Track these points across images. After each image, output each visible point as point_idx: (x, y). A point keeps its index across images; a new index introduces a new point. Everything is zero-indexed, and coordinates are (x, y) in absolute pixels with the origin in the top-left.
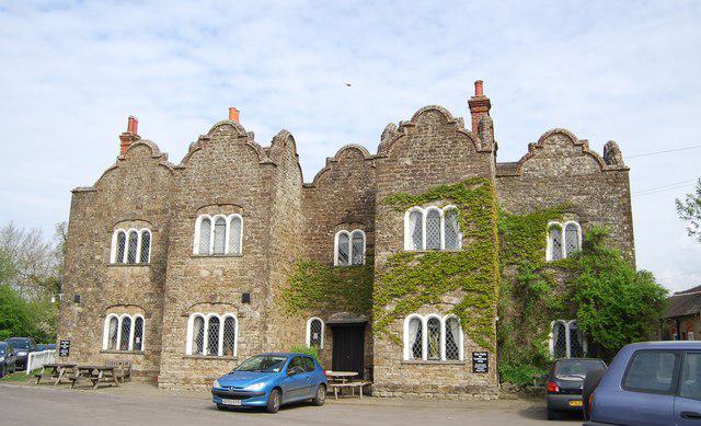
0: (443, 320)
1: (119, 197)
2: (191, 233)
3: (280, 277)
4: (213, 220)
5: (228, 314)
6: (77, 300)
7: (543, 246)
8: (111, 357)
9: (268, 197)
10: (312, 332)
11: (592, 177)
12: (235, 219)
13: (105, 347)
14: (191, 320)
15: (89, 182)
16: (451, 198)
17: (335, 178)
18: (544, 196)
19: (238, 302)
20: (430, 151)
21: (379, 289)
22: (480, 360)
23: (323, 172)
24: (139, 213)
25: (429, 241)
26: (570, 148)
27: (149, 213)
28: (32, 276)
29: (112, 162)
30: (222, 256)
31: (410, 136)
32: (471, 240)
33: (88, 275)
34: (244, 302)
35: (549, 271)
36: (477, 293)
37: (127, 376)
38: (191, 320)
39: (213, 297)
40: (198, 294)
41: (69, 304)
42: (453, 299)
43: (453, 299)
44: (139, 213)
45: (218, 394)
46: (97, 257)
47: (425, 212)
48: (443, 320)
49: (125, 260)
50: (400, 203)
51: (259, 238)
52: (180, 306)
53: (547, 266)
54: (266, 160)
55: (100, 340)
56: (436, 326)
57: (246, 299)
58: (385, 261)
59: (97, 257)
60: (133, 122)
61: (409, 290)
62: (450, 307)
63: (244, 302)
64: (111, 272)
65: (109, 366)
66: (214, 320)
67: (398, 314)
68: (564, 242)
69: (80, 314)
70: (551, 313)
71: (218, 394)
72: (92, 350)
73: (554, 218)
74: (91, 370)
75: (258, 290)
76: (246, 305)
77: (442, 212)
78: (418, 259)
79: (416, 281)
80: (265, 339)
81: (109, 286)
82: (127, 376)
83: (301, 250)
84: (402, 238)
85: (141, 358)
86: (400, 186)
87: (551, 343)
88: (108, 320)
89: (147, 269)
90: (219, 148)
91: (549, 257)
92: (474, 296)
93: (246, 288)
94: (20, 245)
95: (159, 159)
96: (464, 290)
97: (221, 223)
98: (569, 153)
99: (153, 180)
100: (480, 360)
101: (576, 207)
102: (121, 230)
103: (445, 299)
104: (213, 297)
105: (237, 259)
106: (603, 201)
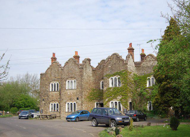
0: (118, 102)
1: (51, 75)
2: (65, 84)
3: (86, 93)
4: (70, 81)
6: (43, 100)
7: (146, 84)
8: (52, 113)
9: (82, 76)
10: (97, 105)
12: (75, 81)
13: (50, 111)
14: (67, 104)
15: (44, 72)
16: (119, 75)
17: (100, 68)
18: (146, 71)
19: (76, 100)
21: (105, 96)
22: (125, 111)
24: (56, 79)
25: (115, 85)
26: (153, 59)
27: (58, 79)
28: (35, 91)
29: (49, 66)
30: (72, 89)
31: (110, 61)
32: (123, 84)
33: (45, 94)
34: (77, 100)
35: (147, 89)
36: (125, 97)
37: (55, 117)
38: (67, 104)
39: (71, 99)
42: (119, 98)
43: (119, 98)
44: (56, 79)
45: (67, 118)
46: (47, 90)
47: (114, 78)
48: (118, 102)
49: (53, 90)
50: (109, 76)
51: (80, 86)
52: (64, 101)
53: (147, 88)
54: (80, 67)
55: (49, 109)
57: (78, 99)
59: (47, 90)
60: (54, 54)
61: (110, 96)
63: (77, 100)
64: (50, 93)
65: (50, 115)
66: (71, 104)
67: (109, 101)
69: (44, 103)
70: (148, 99)
71: (67, 118)
72: (48, 112)
73: (149, 77)
74: (47, 116)
75: (80, 97)
77: (117, 78)
78: (112, 89)
79: (112, 94)
80: (82, 108)
81: (50, 97)
82: (55, 117)
83: (93, 86)
84: (109, 84)
85: (58, 113)
86: (108, 72)
87: (148, 107)
88: (50, 104)
89: (58, 92)
90: (70, 65)
91: (148, 86)
92: (124, 97)
93: (77, 96)
94: (31, 79)
95: (59, 65)
96: (122, 95)
97: (72, 82)
98: (152, 60)
100: (125, 111)
102: (52, 83)
103: (118, 97)
104: (71, 99)
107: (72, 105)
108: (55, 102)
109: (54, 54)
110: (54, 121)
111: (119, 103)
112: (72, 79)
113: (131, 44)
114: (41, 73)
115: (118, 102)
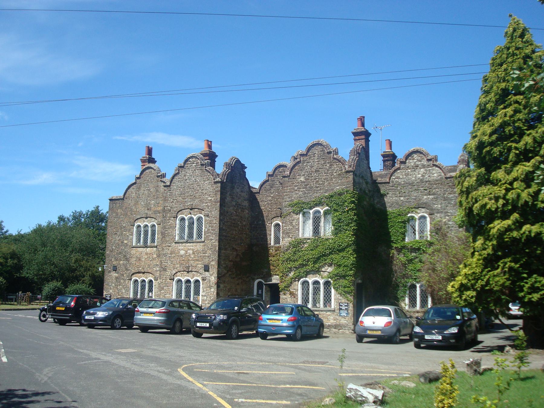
1: (136, 203)
5: (195, 278)
11: (439, 182)
19: (202, 271)
20: (316, 171)
22: (343, 308)
23: (264, 183)
24: (150, 213)
27: (156, 212)
33: (120, 253)
40: (179, 266)
41: (110, 272)
48: (322, 281)
56: (318, 286)
57: (207, 269)
58: (288, 244)
59: (125, 242)
62: (326, 274)
63: (205, 271)
68: (417, 228)
69: (117, 278)
76: (207, 273)
81: (133, 260)
86: (297, 196)
93: (206, 261)
99: (157, 191)
101: (425, 203)
105: (201, 244)
106: (445, 199)
107: (190, 286)
108: (146, 274)
109: (150, 151)
110: (238, 344)
111: (327, 284)
112: (191, 211)
113: (362, 120)
114: (110, 197)
115: (322, 281)
